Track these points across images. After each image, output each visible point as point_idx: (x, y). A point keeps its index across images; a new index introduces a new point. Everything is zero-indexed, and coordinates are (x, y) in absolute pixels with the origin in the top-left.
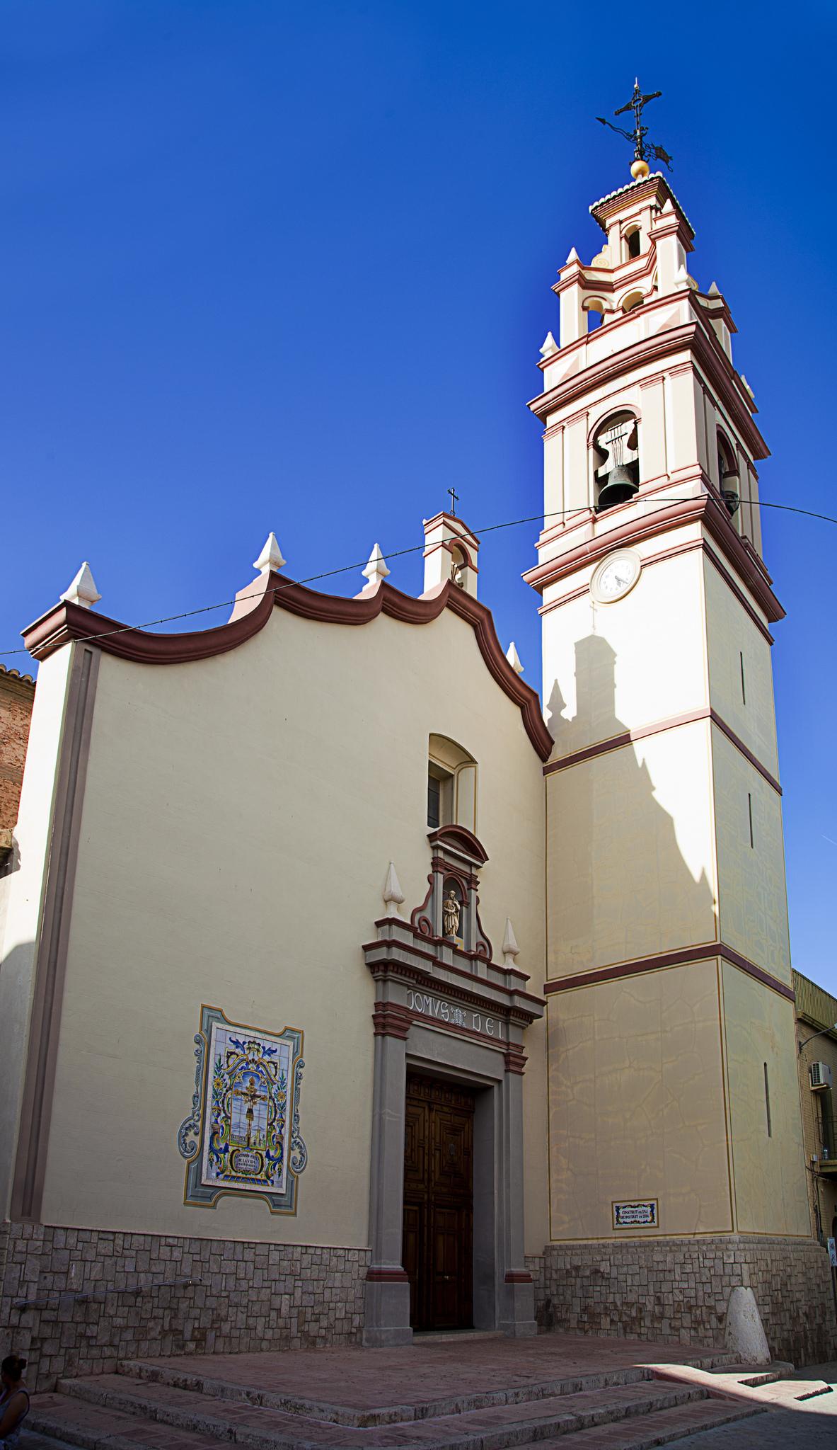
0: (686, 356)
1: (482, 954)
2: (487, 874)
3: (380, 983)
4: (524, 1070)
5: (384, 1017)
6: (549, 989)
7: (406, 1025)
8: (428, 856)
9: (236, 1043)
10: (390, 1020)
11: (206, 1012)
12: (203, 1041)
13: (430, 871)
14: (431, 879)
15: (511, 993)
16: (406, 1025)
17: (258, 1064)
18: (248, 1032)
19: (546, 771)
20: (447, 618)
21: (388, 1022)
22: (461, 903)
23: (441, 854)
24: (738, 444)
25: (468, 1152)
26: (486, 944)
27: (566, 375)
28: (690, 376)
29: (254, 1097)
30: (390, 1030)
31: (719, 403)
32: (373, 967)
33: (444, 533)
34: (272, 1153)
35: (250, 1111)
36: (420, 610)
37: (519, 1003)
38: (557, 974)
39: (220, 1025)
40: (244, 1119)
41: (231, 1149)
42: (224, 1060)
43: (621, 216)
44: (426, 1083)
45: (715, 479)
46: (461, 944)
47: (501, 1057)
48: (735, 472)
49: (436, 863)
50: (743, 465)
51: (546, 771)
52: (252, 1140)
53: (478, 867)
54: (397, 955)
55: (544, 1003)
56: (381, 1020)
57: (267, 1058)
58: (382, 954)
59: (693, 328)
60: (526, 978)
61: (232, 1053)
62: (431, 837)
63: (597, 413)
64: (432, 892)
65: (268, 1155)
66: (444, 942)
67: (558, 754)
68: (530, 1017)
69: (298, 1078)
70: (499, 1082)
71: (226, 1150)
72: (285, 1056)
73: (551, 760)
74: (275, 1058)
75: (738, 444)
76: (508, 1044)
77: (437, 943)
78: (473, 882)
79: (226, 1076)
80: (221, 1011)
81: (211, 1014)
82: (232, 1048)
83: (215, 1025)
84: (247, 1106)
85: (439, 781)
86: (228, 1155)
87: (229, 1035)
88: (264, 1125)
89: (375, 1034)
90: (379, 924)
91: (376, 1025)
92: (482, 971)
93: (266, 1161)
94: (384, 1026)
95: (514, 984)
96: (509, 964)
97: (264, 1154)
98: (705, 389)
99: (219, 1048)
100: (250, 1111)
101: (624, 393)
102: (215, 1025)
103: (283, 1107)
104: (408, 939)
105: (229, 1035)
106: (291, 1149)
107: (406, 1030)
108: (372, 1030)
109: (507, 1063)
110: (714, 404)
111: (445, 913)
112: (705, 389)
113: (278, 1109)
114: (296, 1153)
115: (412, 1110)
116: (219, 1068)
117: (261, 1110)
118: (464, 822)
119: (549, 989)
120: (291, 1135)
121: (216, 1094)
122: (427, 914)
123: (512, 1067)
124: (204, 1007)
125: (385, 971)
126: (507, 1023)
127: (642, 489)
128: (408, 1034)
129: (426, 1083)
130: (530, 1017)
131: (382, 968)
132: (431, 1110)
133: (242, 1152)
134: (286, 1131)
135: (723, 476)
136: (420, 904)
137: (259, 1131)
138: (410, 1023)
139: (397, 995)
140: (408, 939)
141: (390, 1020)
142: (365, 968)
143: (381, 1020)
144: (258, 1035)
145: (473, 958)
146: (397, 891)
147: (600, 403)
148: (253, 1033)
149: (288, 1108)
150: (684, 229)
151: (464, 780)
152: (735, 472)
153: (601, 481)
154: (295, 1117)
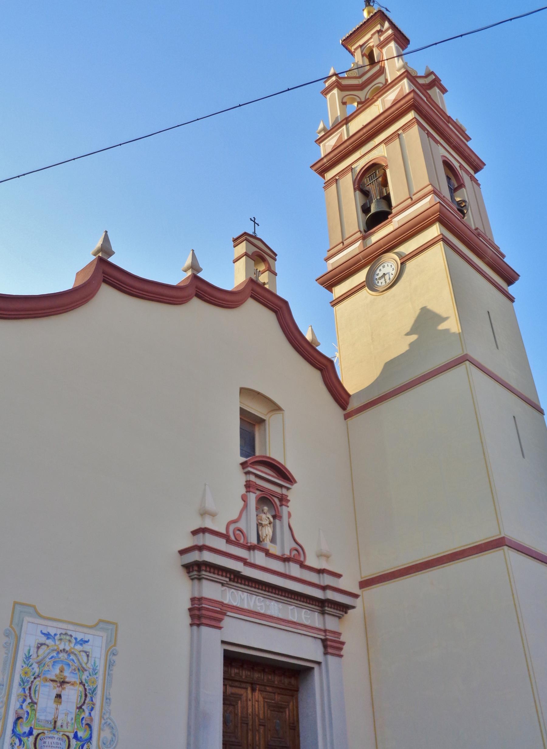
0: (411, 115)
1: (296, 557)
2: (295, 494)
3: (196, 582)
4: (342, 653)
5: (199, 609)
6: (365, 584)
7: (219, 616)
8: (242, 479)
9: (48, 635)
10: (204, 612)
11: (18, 608)
12: (14, 635)
13: (243, 490)
14: (244, 498)
15: (324, 588)
16: (219, 616)
17: (69, 653)
18: (60, 625)
19: (347, 417)
20: (251, 305)
21: (202, 614)
22: (274, 517)
23: (252, 478)
24: (461, 166)
25: (294, 727)
26: (299, 549)
27: (335, 145)
28: (416, 127)
29: (63, 683)
30: (204, 621)
31: (442, 141)
32: (188, 568)
33: (247, 247)
34: (80, 734)
35: (59, 696)
36: (228, 297)
37: (331, 595)
38: (370, 572)
39: (31, 619)
40: (51, 704)
41: (35, 732)
42: (33, 651)
43: (361, 42)
44: (239, 664)
45: (446, 193)
46: (274, 549)
47: (319, 643)
48: (461, 185)
49: (249, 486)
50: (466, 179)
51: (347, 417)
52: (59, 724)
53: (288, 489)
54: (208, 557)
55: (356, 596)
56: (196, 612)
57: (78, 647)
58: (195, 556)
59: (412, 95)
60: (339, 576)
61: (42, 644)
62: (244, 465)
63: (360, 166)
64: (246, 506)
65: (76, 736)
66: (259, 546)
67: (353, 405)
68: (345, 608)
69: (110, 665)
70: (319, 663)
71: (30, 733)
72: (97, 647)
73: (350, 408)
74: (86, 647)
75: (461, 166)
76: (325, 631)
77: (250, 548)
78: (284, 500)
79: (35, 666)
80: (34, 607)
81: (22, 609)
82: (43, 639)
83: (27, 619)
84: (55, 692)
85: (250, 425)
86: (32, 739)
87: (40, 628)
88: (73, 709)
89: (191, 625)
90: (195, 533)
91: (192, 616)
92: (294, 570)
93: (73, 742)
94: (199, 617)
95: (327, 580)
96: (323, 565)
97: (71, 735)
98: (429, 134)
99: (30, 638)
100: (59, 696)
101: (377, 151)
102: (27, 619)
103: (94, 691)
104: (220, 544)
105: (40, 628)
106: (100, 730)
107: (220, 620)
108: (188, 621)
109: (325, 647)
110: (437, 142)
111: (259, 525)
112: (429, 134)
113: (87, 694)
114: (106, 734)
115: (230, 690)
116: (28, 657)
117: (72, 695)
118: (274, 453)
119: (365, 584)
120: (101, 717)
121: (23, 682)
122: (242, 525)
123: (330, 650)
124: (15, 603)
125: (199, 571)
126: (323, 613)
127: (394, 211)
128: (222, 624)
129: (239, 664)
130: (345, 608)
131: (196, 568)
132: (253, 690)
133: (47, 734)
134: (96, 715)
135: (453, 191)
136: (235, 517)
137: (67, 715)
138: (225, 614)
139: (212, 590)
140: (220, 544)
141: (204, 612)
142: (181, 568)
143: (196, 612)
144: (71, 627)
145: (285, 560)
146: (210, 505)
147: (359, 160)
148: (65, 626)
149: (99, 692)
150: (398, 35)
151: (273, 423)
152: (461, 185)
153: (366, 209)
154: (107, 699)
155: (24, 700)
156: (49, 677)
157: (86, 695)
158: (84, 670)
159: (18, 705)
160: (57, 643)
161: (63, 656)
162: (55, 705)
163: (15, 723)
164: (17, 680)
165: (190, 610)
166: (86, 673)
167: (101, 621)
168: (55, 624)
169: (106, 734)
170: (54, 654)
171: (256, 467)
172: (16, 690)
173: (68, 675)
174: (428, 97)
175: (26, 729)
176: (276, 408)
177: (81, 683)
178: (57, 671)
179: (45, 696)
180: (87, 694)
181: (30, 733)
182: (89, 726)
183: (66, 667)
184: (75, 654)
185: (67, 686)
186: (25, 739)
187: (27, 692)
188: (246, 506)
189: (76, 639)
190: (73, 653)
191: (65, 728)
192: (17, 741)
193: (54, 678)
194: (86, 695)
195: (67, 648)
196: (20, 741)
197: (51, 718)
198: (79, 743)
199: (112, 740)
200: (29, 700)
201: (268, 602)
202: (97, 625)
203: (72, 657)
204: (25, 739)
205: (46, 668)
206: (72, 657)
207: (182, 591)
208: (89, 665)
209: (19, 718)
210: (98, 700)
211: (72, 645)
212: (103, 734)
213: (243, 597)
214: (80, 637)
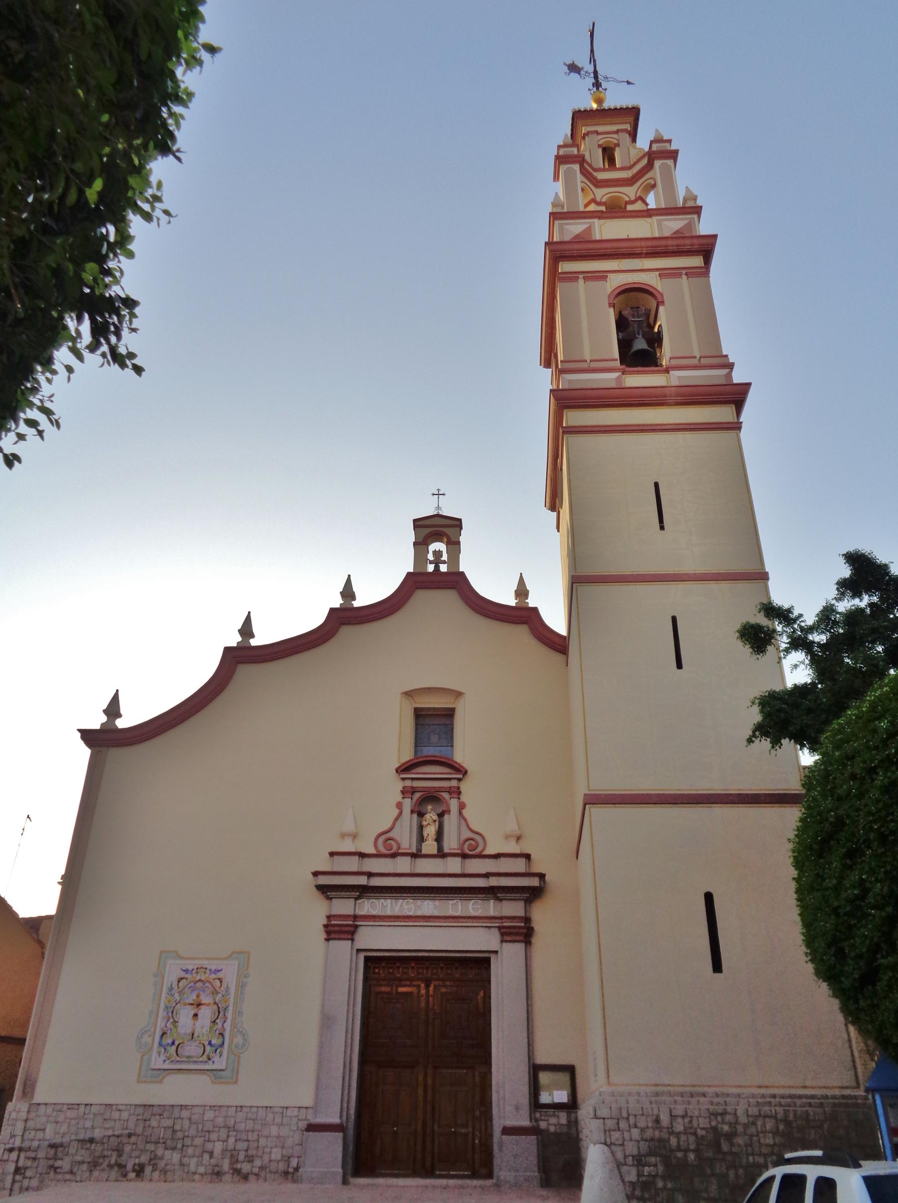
9: (186, 971)
12: (160, 974)
14: (399, 805)
15: (487, 875)
21: (339, 930)
29: (199, 1005)
34: (213, 1042)
35: (196, 1015)
41: (177, 1043)
52: (196, 1035)
57: (213, 976)
61: (182, 979)
65: (210, 1043)
70: (496, 952)
72: (230, 975)
74: (220, 975)
80: (176, 952)
82: (183, 974)
84: (192, 1013)
86: (174, 1048)
88: (208, 1023)
89: (327, 940)
97: (206, 1043)
100: (196, 1015)
113: (220, 1012)
116: (171, 989)
117: (206, 1014)
134: (227, 1026)
149: (231, 1008)
155: (168, 1021)
156: (187, 1001)
157: (219, 1012)
158: (217, 993)
159: (163, 1025)
160: (194, 975)
161: (199, 985)
162: (192, 1022)
163: (162, 1036)
164: (162, 1006)
165: (325, 926)
166: (220, 995)
167: (233, 952)
168: (192, 962)
169: (239, 1040)
170: (192, 984)
171: (414, 771)
172: (162, 1013)
173: (205, 999)
174: (599, 214)
175: (170, 1041)
176: (459, 694)
177: (215, 1003)
178: (195, 997)
179: (185, 1016)
180: (220, 1012)
181: (173, 1043)
182: (222, 1034)
183: (201, 993)
184: (210, 983)
185: (202, 1007)
186: (169, 1048)
187: (170, 1015)
188: (401, 813)
189: (210, 970)
190: (208, 981)
191: (201, 1038)
192: (163, 1050)
193: (191, 1002)
194: (219, 1012)
195: (203, 978)
196: (165, 1049)
197: (190, 1031)
198: (213, 1049)
199: (244, 1045)
200: (171, 1020)
201: (419, 902)
202: (231, 955)
203: (207, 984)
204: (169, 1048)
205: (185, 996)
206: (207, 984)
207: (318, 911)
208: (222, 988)
209: (164, 1034)
210: (229, 1015)
211: (207, 975)
212: (235, 1040)
213: (385, 904)
214: (213, 968)
